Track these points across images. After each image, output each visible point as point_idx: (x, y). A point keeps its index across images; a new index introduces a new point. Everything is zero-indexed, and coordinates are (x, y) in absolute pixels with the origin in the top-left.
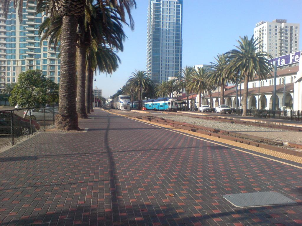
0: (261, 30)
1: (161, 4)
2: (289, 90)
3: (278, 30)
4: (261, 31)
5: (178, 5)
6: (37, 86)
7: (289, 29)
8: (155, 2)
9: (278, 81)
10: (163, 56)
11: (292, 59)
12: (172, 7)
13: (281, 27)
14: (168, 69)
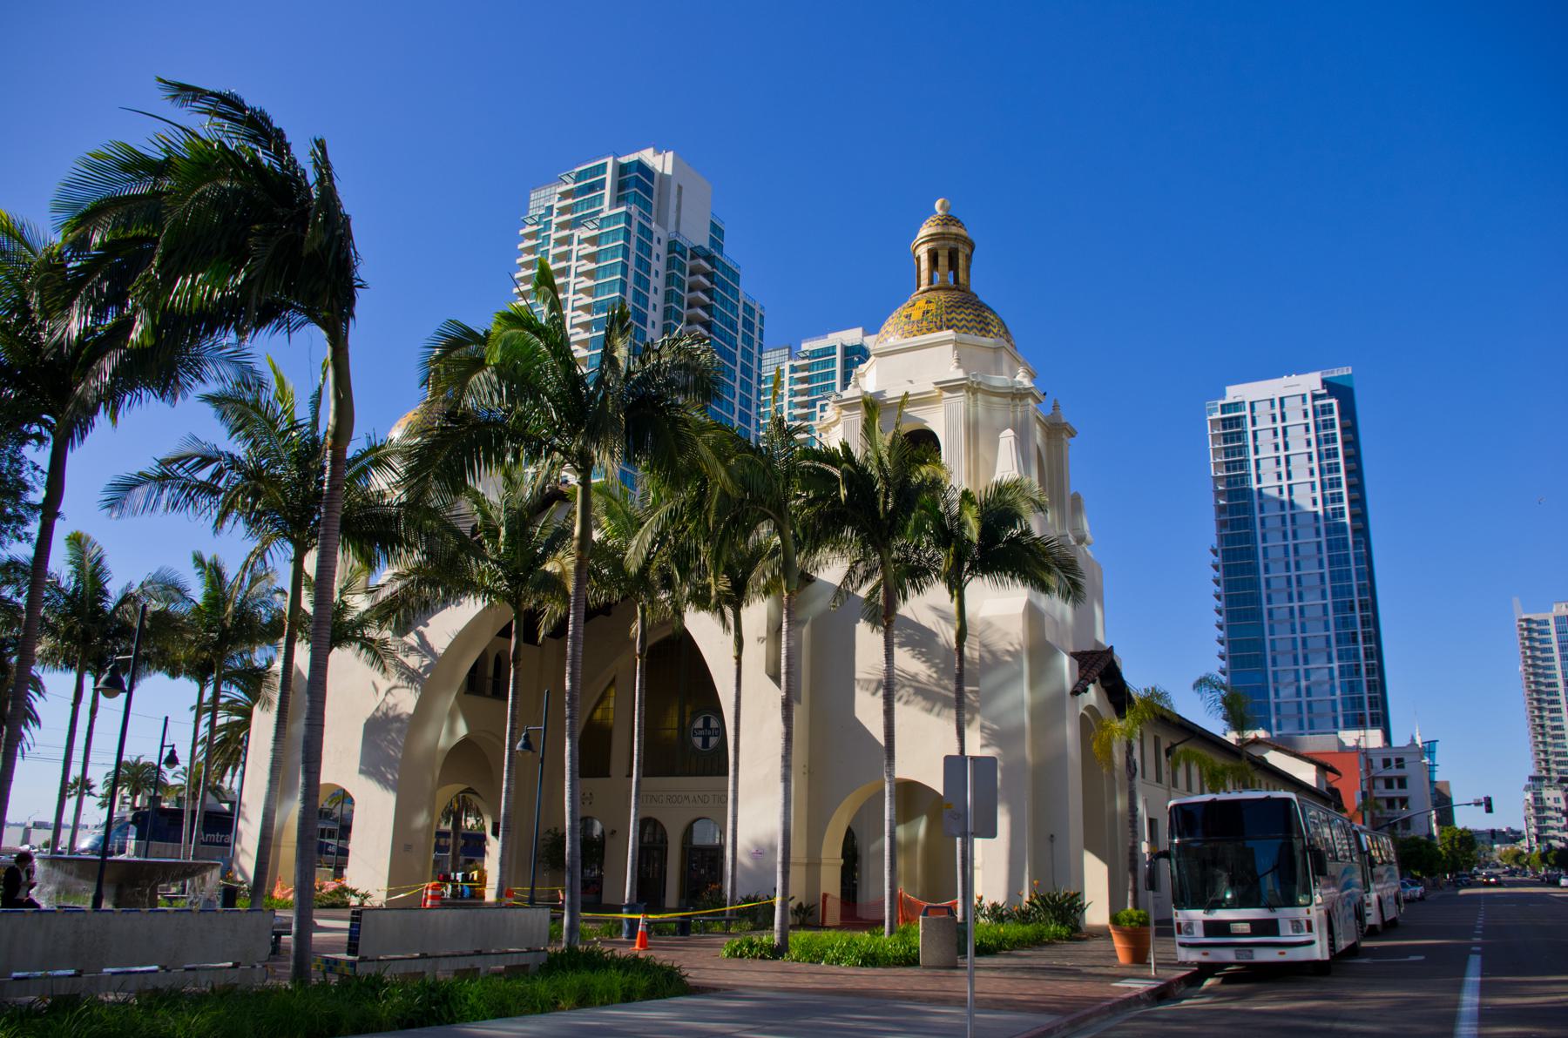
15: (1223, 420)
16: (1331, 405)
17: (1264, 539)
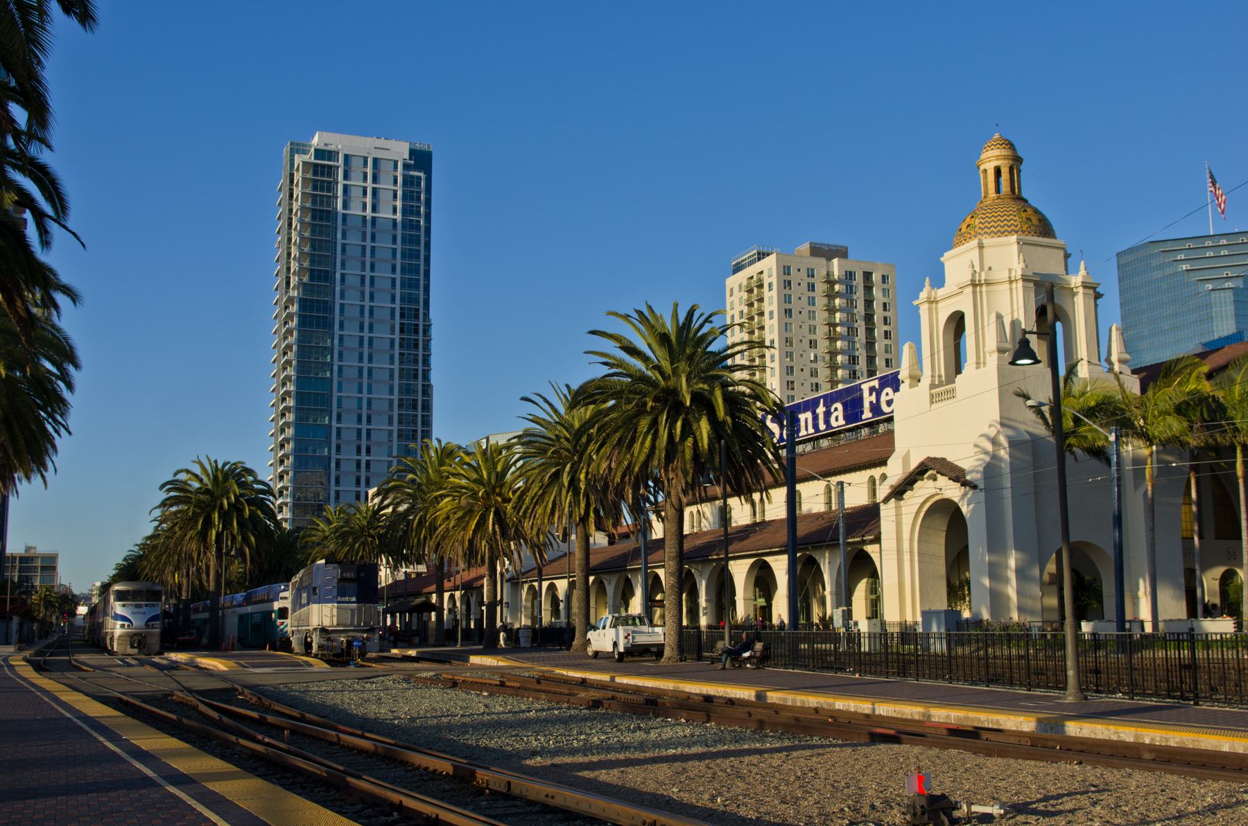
0: (754, 283)
1: (338, 167)
2: (863, 536)
3: (821, 288)
4: (755, 288)
5: (412, 173)
6: (977, 622)
7: (859, 281)
8: (313, 160)
9: (813, 497)
10: (345, 394)
11: (871, 403)
12: (385, 185)
13: (828, 274)
14: (368, 451)
15: (316, 165)
16: (419, 178)
17: (342, 296)
